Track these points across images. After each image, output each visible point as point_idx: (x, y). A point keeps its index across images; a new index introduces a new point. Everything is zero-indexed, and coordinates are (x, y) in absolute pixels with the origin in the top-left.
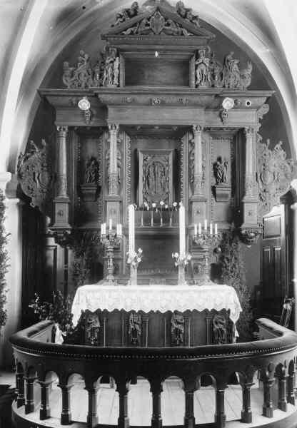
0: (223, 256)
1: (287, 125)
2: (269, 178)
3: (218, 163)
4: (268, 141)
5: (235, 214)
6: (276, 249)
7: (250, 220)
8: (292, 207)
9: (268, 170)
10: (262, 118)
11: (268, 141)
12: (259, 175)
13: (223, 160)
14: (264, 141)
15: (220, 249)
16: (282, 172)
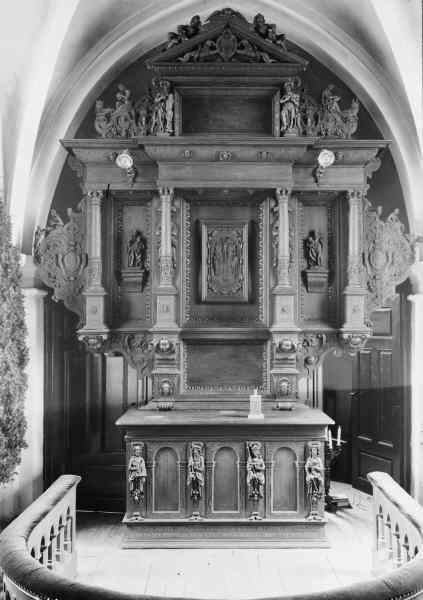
3: (311, 239)
4: (380, 209)
9: (381, 249)
11: (380, 209)
12: (367, 256)
13: (316, 234)
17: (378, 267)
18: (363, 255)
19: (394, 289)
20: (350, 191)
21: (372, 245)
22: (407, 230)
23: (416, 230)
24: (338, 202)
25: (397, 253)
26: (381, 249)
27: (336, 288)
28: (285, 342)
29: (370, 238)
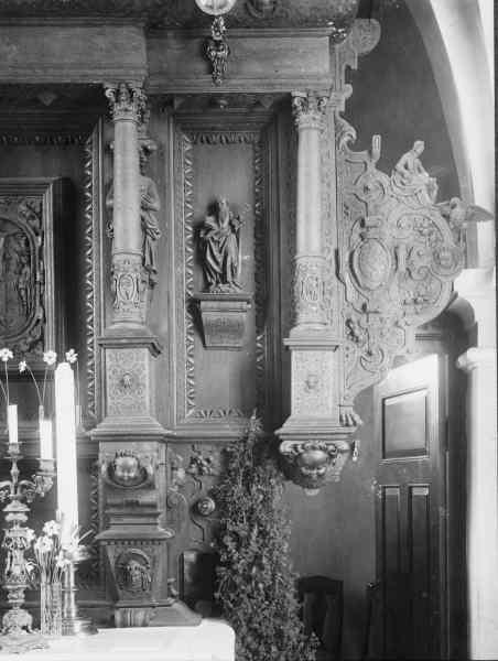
0: (224, 527)
1: (435, 59)
2: (379, 266)
3: (210, 221)
4: (377, 140)
5: (267, 393)
6: (416, 492)
7: (318, 394)
8: (461, 361)
9: (379, 241)
10: (355, 66)
11: (377, 140)
12: (345, 258)
13: (224, 208)
14: (362, 143)
15: (212, 505)
16: (422, 247)
20: (298, 94)
22: (450, 186)
23: (480, 184)
24: (275, 123)
26: (379, 241)
28: (120, 461)
29: (356, 215)
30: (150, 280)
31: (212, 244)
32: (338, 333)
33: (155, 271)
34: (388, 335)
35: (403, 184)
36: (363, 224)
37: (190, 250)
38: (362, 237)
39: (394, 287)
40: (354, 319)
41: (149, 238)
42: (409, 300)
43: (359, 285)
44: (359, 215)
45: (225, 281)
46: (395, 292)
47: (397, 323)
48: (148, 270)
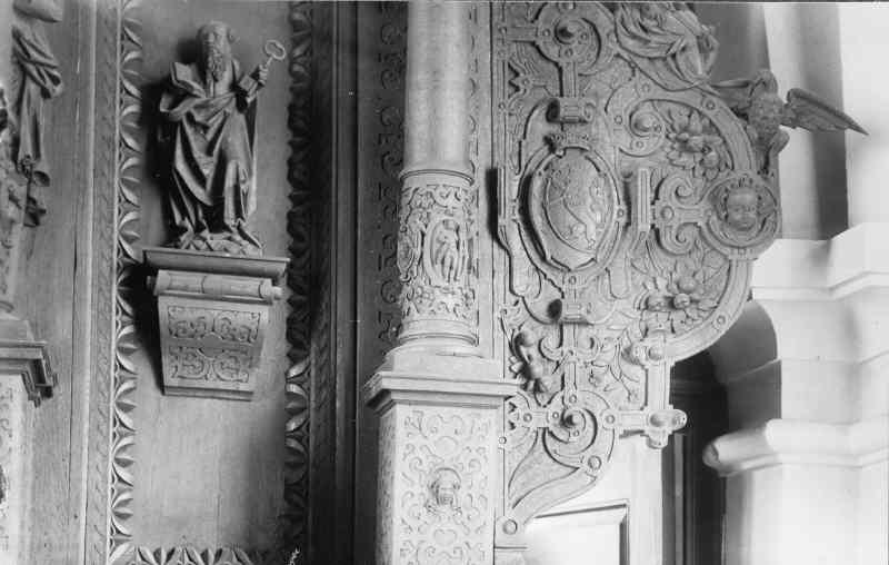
3: (185, 73)
12: (510, 189)
13: (220, 47)
17: (577, 259)
18: (492, 177)
19: (661, 384)
21: (540, 127)
25: (676, 179)
27: (326, 367)
30: (30, 199)
31: (189, 130)
32: (496, 367)
33: (43, 177)
34: (608, 379)
35: (645, 29)
36: (552, 113)
37: (130, 142)
38: (550, 143)
39: (620, 264)
40: (532, 338)
41: (32, 87)
42: (658, 298)
43: (543, 258)
44: (542, 93)
45: (217, 224)
46: (621, 280)
47: (628, 351)
48: (25, 171)
